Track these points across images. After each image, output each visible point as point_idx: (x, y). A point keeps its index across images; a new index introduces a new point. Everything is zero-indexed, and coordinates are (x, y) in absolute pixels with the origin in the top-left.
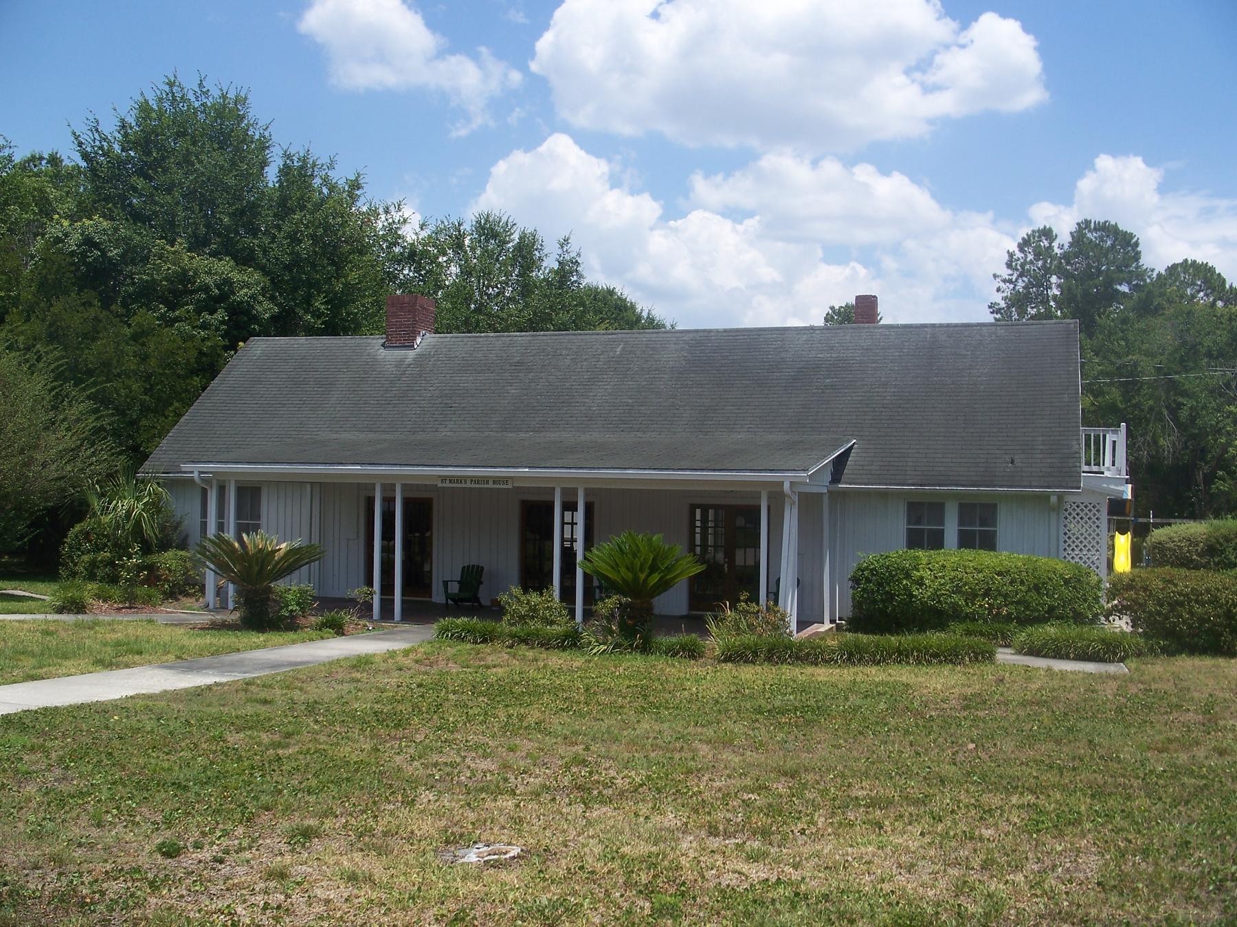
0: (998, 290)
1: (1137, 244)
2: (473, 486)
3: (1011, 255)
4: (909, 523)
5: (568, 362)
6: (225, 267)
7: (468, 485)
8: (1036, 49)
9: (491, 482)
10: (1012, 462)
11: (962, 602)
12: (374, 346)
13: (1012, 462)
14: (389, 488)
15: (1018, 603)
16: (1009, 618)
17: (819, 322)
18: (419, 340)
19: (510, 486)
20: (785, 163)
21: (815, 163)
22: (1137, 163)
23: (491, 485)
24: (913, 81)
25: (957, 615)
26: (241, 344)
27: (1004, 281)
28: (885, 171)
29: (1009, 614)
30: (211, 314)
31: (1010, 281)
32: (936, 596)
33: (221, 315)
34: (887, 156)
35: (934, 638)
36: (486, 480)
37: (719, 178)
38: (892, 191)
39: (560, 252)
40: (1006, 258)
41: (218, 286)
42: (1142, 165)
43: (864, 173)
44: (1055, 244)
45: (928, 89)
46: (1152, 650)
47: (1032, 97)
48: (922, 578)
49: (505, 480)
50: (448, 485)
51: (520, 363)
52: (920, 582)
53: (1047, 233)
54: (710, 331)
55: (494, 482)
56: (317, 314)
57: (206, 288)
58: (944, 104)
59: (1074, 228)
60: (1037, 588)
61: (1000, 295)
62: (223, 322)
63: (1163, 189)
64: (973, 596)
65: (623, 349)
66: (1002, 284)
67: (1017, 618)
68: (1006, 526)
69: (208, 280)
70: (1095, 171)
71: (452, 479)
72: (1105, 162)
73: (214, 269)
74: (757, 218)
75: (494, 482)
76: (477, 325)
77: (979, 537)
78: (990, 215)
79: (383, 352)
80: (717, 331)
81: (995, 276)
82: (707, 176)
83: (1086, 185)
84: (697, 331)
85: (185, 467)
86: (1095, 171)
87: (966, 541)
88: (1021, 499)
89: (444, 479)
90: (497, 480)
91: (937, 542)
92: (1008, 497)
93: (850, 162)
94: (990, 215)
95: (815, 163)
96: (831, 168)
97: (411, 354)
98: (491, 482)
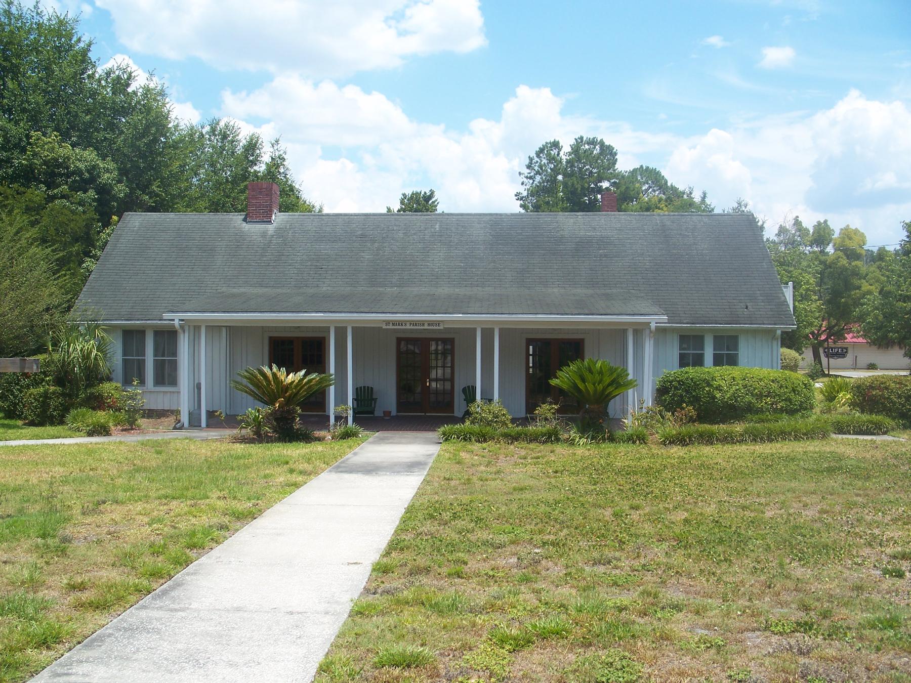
0: (523, 184)
1: (616, 154)
2: (412, 327)
3: (531, 159)
4: (714, 350)
5: (401, 235)
6: (90, 155)
7: (408, 327)
8: (480, 8)
9: (426, 325)
10: (747, 308)
11: (754, 401)
12: (237, 219)
13: (747, 308)
14: (341, 332)
15: (785, 400)
16: (782, 410)
17: (396, 206)
18: (273, 217)
19: (441, 327)
20: (292, 83)
21: (316, 85)
22: (546, 92)
23: (426, 327)
24: (390, 27)
25: (750, 409)
26: (115, 218)
27: (527, 177)
28: (367, 91)
29: (782, 407)
30: (85, 193)
31: (531, 178)
32: (734, 396)
33: (91, 193)
34: (367, 81)
35: (738, 428)
36: (422, 323)
37: (244, 93)
38: (377, 107)
39: (272, 150)
40: (527, 162)
41: (88, 171)
42: (550, 95)
43: (352, 92)
44: (562, 153)
45: (402, 33)
46: (898, 427)
47: (475, 42)
48: (720, 386)
49: (438, 323)
50: (391, 327)
51: (363, 236)
52: (718, 388)
53: (556, 145)
54: (501, 215)
55: (429, 325)
56: (152, 194)
57: (78, 172)
58: (413, 45)
59: (573, 142)
60: (794, 391)
61: (524, 187)
62: (94, 200)
63: (563, 112)
64: (760, 396)
65: (440, 226)
66: (525, 180)
67: (786, 410)
68: (744, 351)
69: (81, 166)
70: (516, 97)
71: (394, 323)
72: (523, 91)
73: (84, 158)
74: (272, 124)
75: (429, 325)
76: (223, 206)
77: (727, 356)
78: (442, 126)
79: (246, 227)
80: (506, 215)
81: (520, 174)
82: (234, 93)
83: (509, 107)
84: (491, 215)
85: (167, 316)
86: (516, 97)
87: (718, 361)
88: (755, 332)
89: (387, 322)
90: (431, 323)
91: (698, 361)
92: (747, 331)
93: (341, 84)
94: (442, 126)
95: (316, 85)
96: (328, 88)
97: (271, 228)
98: (426, 325)
